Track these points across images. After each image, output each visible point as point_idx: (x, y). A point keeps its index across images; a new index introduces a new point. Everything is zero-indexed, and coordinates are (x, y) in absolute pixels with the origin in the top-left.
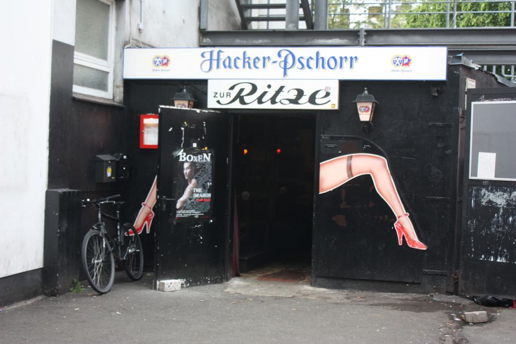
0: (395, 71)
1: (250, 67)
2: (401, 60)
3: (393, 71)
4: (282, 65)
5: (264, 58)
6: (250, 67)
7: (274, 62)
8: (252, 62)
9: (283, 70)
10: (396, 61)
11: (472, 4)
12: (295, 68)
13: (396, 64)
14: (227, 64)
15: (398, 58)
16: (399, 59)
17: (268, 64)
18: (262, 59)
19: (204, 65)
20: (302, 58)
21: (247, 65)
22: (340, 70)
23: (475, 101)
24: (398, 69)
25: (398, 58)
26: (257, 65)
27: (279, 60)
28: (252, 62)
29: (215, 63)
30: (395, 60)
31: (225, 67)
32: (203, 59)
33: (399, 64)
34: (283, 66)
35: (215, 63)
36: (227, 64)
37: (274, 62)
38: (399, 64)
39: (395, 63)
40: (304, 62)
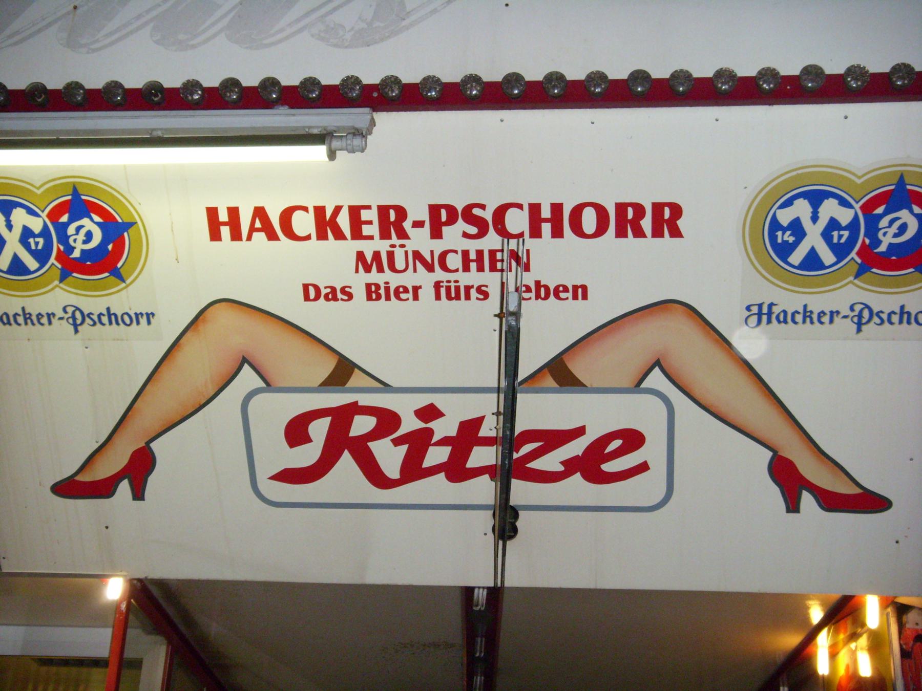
0: (783, 319)
1: (812, 322)
2: (845, 216)
3: (487, 286)
4: (856, 319)
5: (832, 313)
6: (812, 322)
7: (846, 317)
8: (815, 317)
9: (855, 326)
10: (797, 228)
11: (908, 652)
12: (871, 324)
13: (797, 257)
14: (782, 319)
15: (816, 198)
16: (830, 209)
17: (836, 319)
18: (829, 314)
19: (749, 321)
20: (882, 312)
21: (808, 320)
22: (829, 325)
23: (856, 183)
24: (818, 302)
25: (816, 198)
26: (823, 320)
27: (852, 314)
28: (815, 317)
29: (765, 318)
30: (785, 217)
31: (779, 322)
32: (749, 313)
33: (827, 256)
34: (856, 321)
35: (765, 318)
36: (782, 319)
37: (846, 317)
38: (827, 256)
39: (784, 251)
40: (885, 316)
